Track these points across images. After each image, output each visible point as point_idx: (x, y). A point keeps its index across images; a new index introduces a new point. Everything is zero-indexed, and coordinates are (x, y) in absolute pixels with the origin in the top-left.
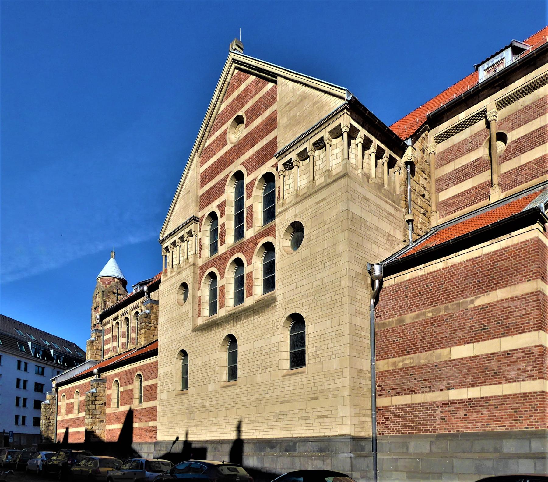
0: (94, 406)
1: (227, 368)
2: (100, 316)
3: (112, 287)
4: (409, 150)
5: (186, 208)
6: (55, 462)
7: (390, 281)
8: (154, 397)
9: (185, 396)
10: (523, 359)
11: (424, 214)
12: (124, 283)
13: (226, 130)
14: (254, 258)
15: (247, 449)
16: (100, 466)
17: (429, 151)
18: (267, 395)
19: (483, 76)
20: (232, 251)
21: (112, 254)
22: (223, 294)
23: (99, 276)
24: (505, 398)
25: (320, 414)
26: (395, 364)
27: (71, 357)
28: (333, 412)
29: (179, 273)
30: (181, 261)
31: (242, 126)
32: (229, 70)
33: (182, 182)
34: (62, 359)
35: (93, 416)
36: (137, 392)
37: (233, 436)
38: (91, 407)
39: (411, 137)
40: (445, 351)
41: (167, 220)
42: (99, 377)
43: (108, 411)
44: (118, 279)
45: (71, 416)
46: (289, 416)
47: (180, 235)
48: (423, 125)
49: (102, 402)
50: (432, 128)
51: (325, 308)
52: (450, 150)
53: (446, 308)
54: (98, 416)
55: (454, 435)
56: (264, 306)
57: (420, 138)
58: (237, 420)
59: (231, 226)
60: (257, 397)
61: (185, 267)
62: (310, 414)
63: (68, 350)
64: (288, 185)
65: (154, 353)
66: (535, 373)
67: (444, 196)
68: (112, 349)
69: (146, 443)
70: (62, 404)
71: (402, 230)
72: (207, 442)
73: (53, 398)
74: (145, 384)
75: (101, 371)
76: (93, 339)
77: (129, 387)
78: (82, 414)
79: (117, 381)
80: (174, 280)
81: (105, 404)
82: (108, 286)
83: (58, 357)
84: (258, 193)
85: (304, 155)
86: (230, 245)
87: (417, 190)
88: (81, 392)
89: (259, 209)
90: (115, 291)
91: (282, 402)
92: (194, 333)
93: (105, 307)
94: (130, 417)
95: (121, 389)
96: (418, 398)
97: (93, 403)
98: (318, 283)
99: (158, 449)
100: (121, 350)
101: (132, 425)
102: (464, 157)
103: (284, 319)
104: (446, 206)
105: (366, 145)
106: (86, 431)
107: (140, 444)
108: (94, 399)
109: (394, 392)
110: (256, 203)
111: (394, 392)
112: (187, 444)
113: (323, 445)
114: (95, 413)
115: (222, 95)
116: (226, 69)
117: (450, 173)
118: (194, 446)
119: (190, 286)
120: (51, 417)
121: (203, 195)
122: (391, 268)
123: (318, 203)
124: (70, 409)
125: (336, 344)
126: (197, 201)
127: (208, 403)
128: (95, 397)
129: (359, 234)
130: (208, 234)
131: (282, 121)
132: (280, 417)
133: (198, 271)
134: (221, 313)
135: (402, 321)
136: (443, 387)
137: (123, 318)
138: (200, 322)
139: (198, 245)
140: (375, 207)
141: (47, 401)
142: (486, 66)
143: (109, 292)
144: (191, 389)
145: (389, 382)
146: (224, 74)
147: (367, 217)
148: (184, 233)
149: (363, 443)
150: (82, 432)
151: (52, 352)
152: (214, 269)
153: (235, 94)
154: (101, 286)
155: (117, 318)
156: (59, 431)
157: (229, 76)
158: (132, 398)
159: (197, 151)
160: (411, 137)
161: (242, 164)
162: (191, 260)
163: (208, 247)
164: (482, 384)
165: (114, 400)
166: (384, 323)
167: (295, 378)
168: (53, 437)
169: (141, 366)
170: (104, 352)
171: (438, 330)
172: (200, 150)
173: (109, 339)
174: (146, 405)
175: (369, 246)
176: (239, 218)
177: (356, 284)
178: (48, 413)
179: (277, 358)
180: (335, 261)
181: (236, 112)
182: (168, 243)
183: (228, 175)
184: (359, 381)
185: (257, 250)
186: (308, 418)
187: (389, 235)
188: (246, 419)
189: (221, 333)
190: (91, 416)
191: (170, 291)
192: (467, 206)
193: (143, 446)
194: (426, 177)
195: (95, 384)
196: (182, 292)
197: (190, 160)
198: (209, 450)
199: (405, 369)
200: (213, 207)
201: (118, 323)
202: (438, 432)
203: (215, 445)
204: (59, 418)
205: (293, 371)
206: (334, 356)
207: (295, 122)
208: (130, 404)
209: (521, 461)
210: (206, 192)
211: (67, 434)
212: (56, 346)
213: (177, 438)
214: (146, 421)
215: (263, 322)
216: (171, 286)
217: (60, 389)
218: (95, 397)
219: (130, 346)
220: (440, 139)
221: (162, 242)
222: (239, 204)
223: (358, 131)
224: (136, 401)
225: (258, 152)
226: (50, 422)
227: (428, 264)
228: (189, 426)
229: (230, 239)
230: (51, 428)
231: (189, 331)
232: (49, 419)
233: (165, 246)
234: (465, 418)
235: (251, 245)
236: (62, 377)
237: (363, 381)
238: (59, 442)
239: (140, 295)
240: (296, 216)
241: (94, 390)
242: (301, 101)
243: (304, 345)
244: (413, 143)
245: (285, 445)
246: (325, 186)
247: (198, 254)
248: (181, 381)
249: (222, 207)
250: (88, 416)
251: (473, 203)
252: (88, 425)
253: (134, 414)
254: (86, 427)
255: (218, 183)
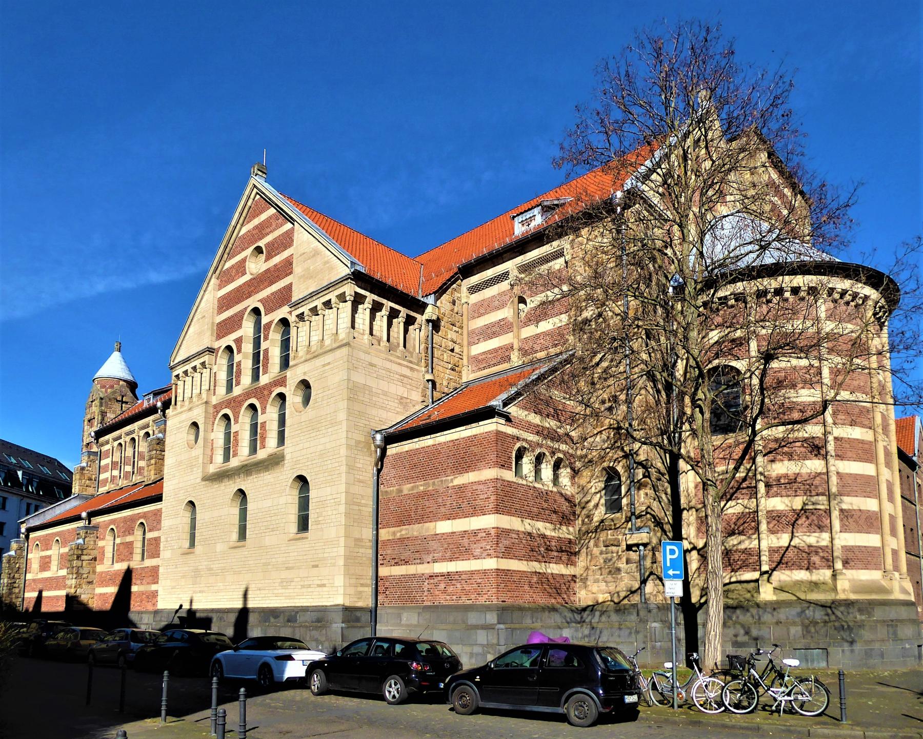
0: (79, 563)
1: (237, 526)
2: (96, 432)
3: (114, 392)
4: (429, 309)
5: (200, 334)
6: (24, 635)
7: (392, 450)
8: (156, 554)
9: (191, 556)
10: (484, 539)
11: (453, 370)
12: (132, 386)
13: (246, 257)
14: (268, 406)
15: (252, 619)
16: (81, 639)
17: (463, 301)
18: (274, 560)
19: (519, 230)
20: (247, 394)
21: (116, 346)
22: (236, 440)
23: (97, 376)
24: (472, 573)
25: (319, 582)
26: (394, 534)
27: (52, 484)
28: (331, 581)
29: (190, 409)
30: (194, 396)
31: (263, 257)
32: (248, 197)
33: (197, 304)
34: (35, 484)
35: (79, 575)
36: (138, 546)
37: (239, 605)
38: (75, 563)
39: (435, 293)
40: (431, 525)
41: (179, 343)
42: (89, 523)
43: (99, 568)
44: (124, 381)
45: (46, 574)
46: (293, 584)
47: (193, 364)
48: (456, 274)
49: (91, 557)
50: (465, 278)
51: (326, 474)
52: (481, 304)
53: (434, 483)
54: (85, 576)
55: (437, 607)
56: (275, 461)
57: (450, 290)
58: (244, 586)
59: (247, 366)
60: (264, 561)
61: (197, 403)
62: (311, 583)
63: (45, 470)
64: (300, 336)
65: (158, 498)
66: (491, 552)
67: (477, 349)
68: (111, 479)
69: (146, 612)
70: (34, 556)
71: (420, 390)
72: (212, 610)
73: (20, 548)
74: (149, 535)
75: (91, 515)
76: (84, 464)
77: (129, 539)
78: (63, 572)
79: (112, 529)
80: (184, 416)
81: (95, 559)
82: (109, 390)
83: (30, 482)
84: (275, 336)
85: (314, 311)
86: (246, 386)
87: (443, 345)
88: (63, 540)
89: (275, 354)
90: (119, 398)
91: (287, 568)
92: (204, 483)
93: (103, 419)
94: (127, 578)
95: (118, 541)
96: (410, 569)
97: (78, 557)
98: (321, 447)
99: (158, 618)
100: (122, 483)
101: (130, 588)
102: (493, 314)
103: (291, 480)
104: (479, 361)
105: (376, 308)
106: (67, 596)
107: (139, 613)
108: (80, 552)
109: (393, 562)
110: (272, 347)
111: (393, 562)
112: (191, 612)
113: (319, 615)
114: (81, 571)
115: (242, 218)
116: (247, 192)
117: (481, 328)
118: (198, 615)
119: (201, 426)
120: (17, 576)
121: (220, 323)
122: (391, 438)
123: (324, 366)
124: (45, 564)
125: (335, 512)
126: (212, 329)
127: (215, 566)
128: (82, 550)
129: (362, 402)
130: (225, 368)
131: (297, 269)
132: (285, 584)
133: (211, 410)
134: (234, 462)
135: (400, 491)
136: (429, 560)
137: (128, 439)
138: (212, 469)
139: (212, 379)
140: (384, 372)
141: (12, 553)
142: (520, 218)
143: (110, 400)
144: (198, 548)
145: (389, 552)
146: (245, 198)
147: (372, 383)
148: (197, 363)
149: (358, 614)
150: (62, 596)
151: (20, 473)
152: (227, 411)
153: (256, 221)
154: (98, 391)
155: (120, 437)
156: (27, 595)
157: (251, 201)
158: (131, 553)
159: (215, 272)
160: (435, 293)
161: (260, 301)
162: (204, 396)
163: (225, 383)
164: (457, 559)
165: (109, 553)
166: (386, 492)
167: (299, 543)
168: (18, 602)
169: (145, 513)
170: (99, 483)
171: (427, 503)
172: (218, 272)
173: (107, 465)
174: (149, 563)
175: (374, 412)
176: (256, 357)
177: (356, 452)
178: (12, 569)
179: (284, 521)
180: (336, 428)
181: (256, 241)
182: (179, 371)
183: (246, 309)
184: (357, 550)
185: (271, 399)
186: (309, 586)
187: (402, 398)
188: (253, 586)
189: (231, 487)
190: (75, 576)
191: (178, 428)
192: (494, 365)
193: (144, 615)
194: (457, 329)
195: (82, 532)
196: (193, 431)
197: (207, 281)
198: (214, 620)
199: (402, 540)
200: (229, 340)
201: (120, 444)
202: (426, 603)
203: (221, 615)
204: (29, 576)
205: (299, 536)
206: (332, 524)
207: (308, 276)
208: (129, 560)
209: (479, 631)
210: (223, 321)
211: (39, 598)
212: (27, 464)
213: (181, 606)
214: (148, 583)
215: (272, 480)
216: (180, 423)
217: (32, 535)
218: (82, 550)
219: (136, 479)
220: (473, 290)
221: (172, 368)
222: (257, 343)
223: (366, 297)
224: (137, 557)
225: (276, 292)
226: (15, 583)
227: (421, 438)
228: (194, 592)
229: (246, 379)
230: (17, 590)
231: (199, 480)
232: (13, 578)
233: (175, 373)
234: (445, 591)
235: (266, 392)
236: (36, 518)
237: (361, 550)
238: (27, 610)
239: (152, 411)
240: (305, 373)
241: (81, 541)
242: (314, 256)
243: (308, 510)
244: (437, 299)
245: (287, 614)
246: (330, 350)
247: (212, 389)
248: (189, 537)
249: (239, 341)
250: (71, 576)
251: (499, 363)
252: (71, 587)
253: (133, 574)
254: (68, 590)
255: (236, 315)
